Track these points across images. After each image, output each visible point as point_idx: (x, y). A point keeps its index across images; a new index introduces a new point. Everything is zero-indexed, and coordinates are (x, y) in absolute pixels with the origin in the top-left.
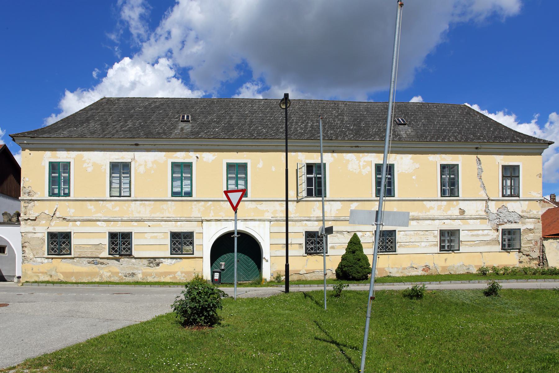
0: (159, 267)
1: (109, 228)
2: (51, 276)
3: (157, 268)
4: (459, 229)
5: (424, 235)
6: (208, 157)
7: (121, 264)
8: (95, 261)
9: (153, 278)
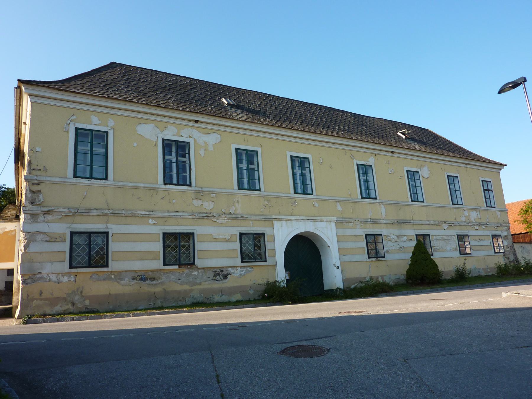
0: (227, 280)
1: (239, 228)
2: (73, 304)
3: (225, 281)
4: (428, 234)
5: (447, 239)
6: (212, 139)
7: (179, 278)
8: (143, 276)
9: (220, 296)
